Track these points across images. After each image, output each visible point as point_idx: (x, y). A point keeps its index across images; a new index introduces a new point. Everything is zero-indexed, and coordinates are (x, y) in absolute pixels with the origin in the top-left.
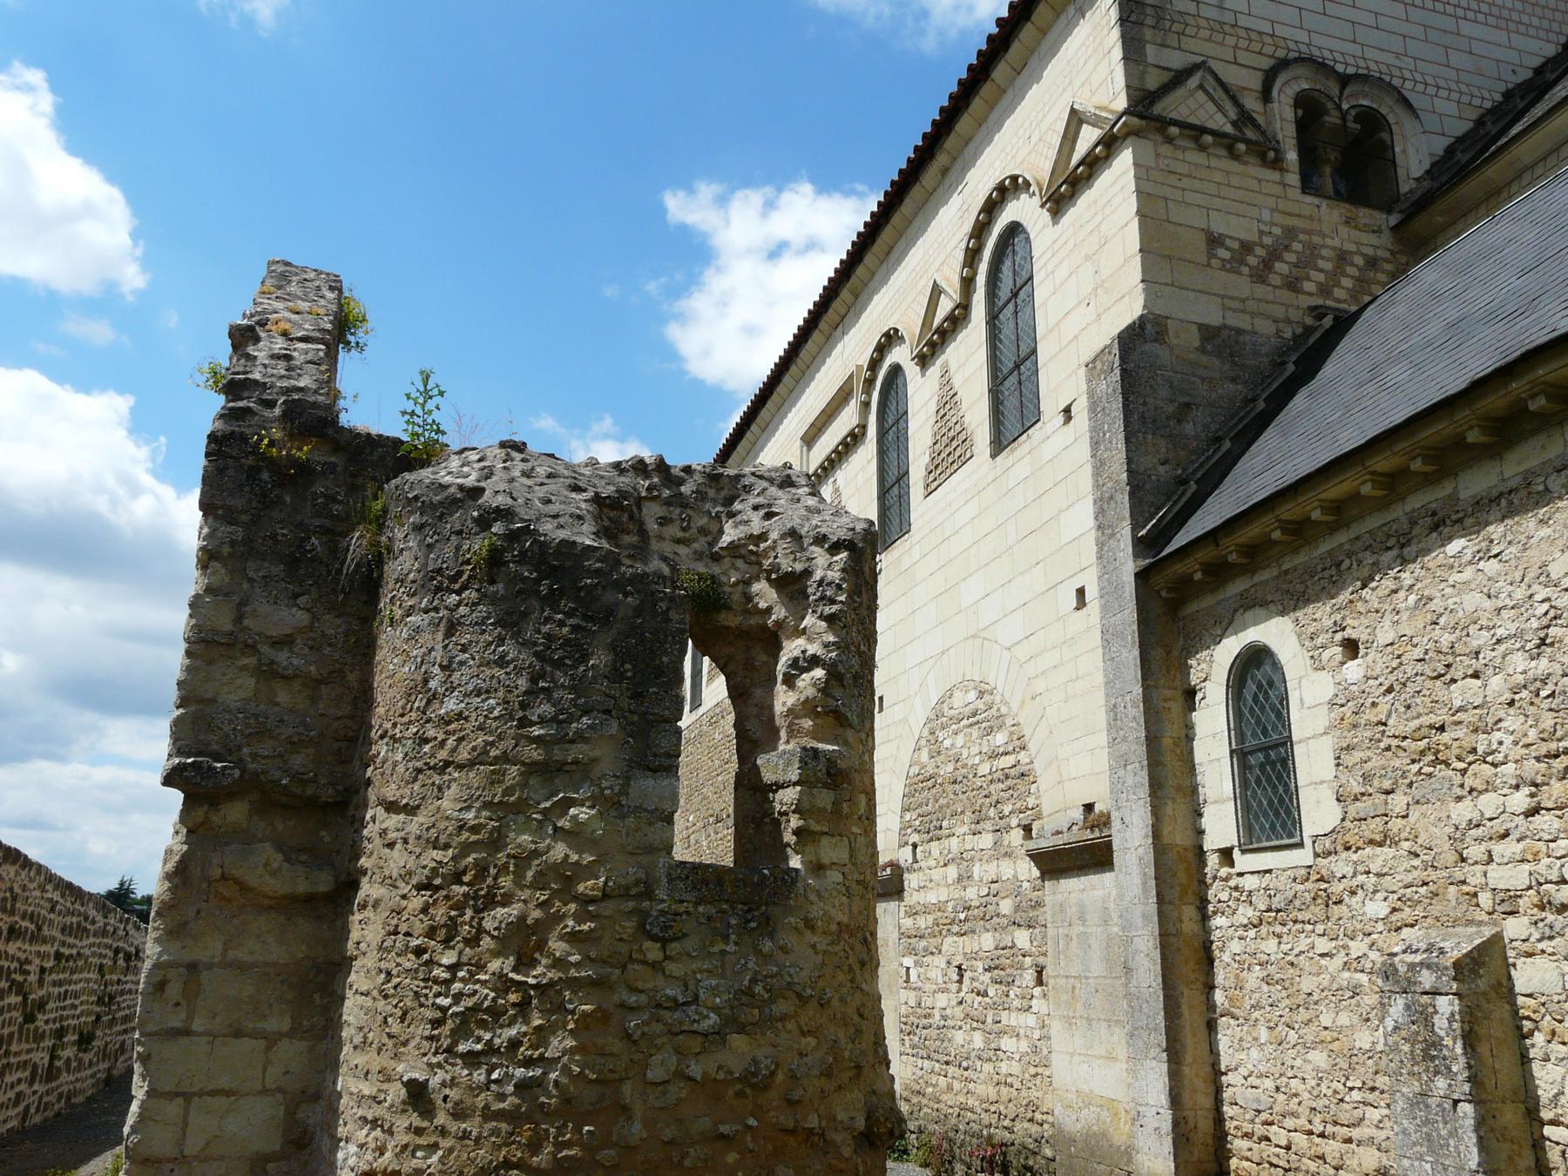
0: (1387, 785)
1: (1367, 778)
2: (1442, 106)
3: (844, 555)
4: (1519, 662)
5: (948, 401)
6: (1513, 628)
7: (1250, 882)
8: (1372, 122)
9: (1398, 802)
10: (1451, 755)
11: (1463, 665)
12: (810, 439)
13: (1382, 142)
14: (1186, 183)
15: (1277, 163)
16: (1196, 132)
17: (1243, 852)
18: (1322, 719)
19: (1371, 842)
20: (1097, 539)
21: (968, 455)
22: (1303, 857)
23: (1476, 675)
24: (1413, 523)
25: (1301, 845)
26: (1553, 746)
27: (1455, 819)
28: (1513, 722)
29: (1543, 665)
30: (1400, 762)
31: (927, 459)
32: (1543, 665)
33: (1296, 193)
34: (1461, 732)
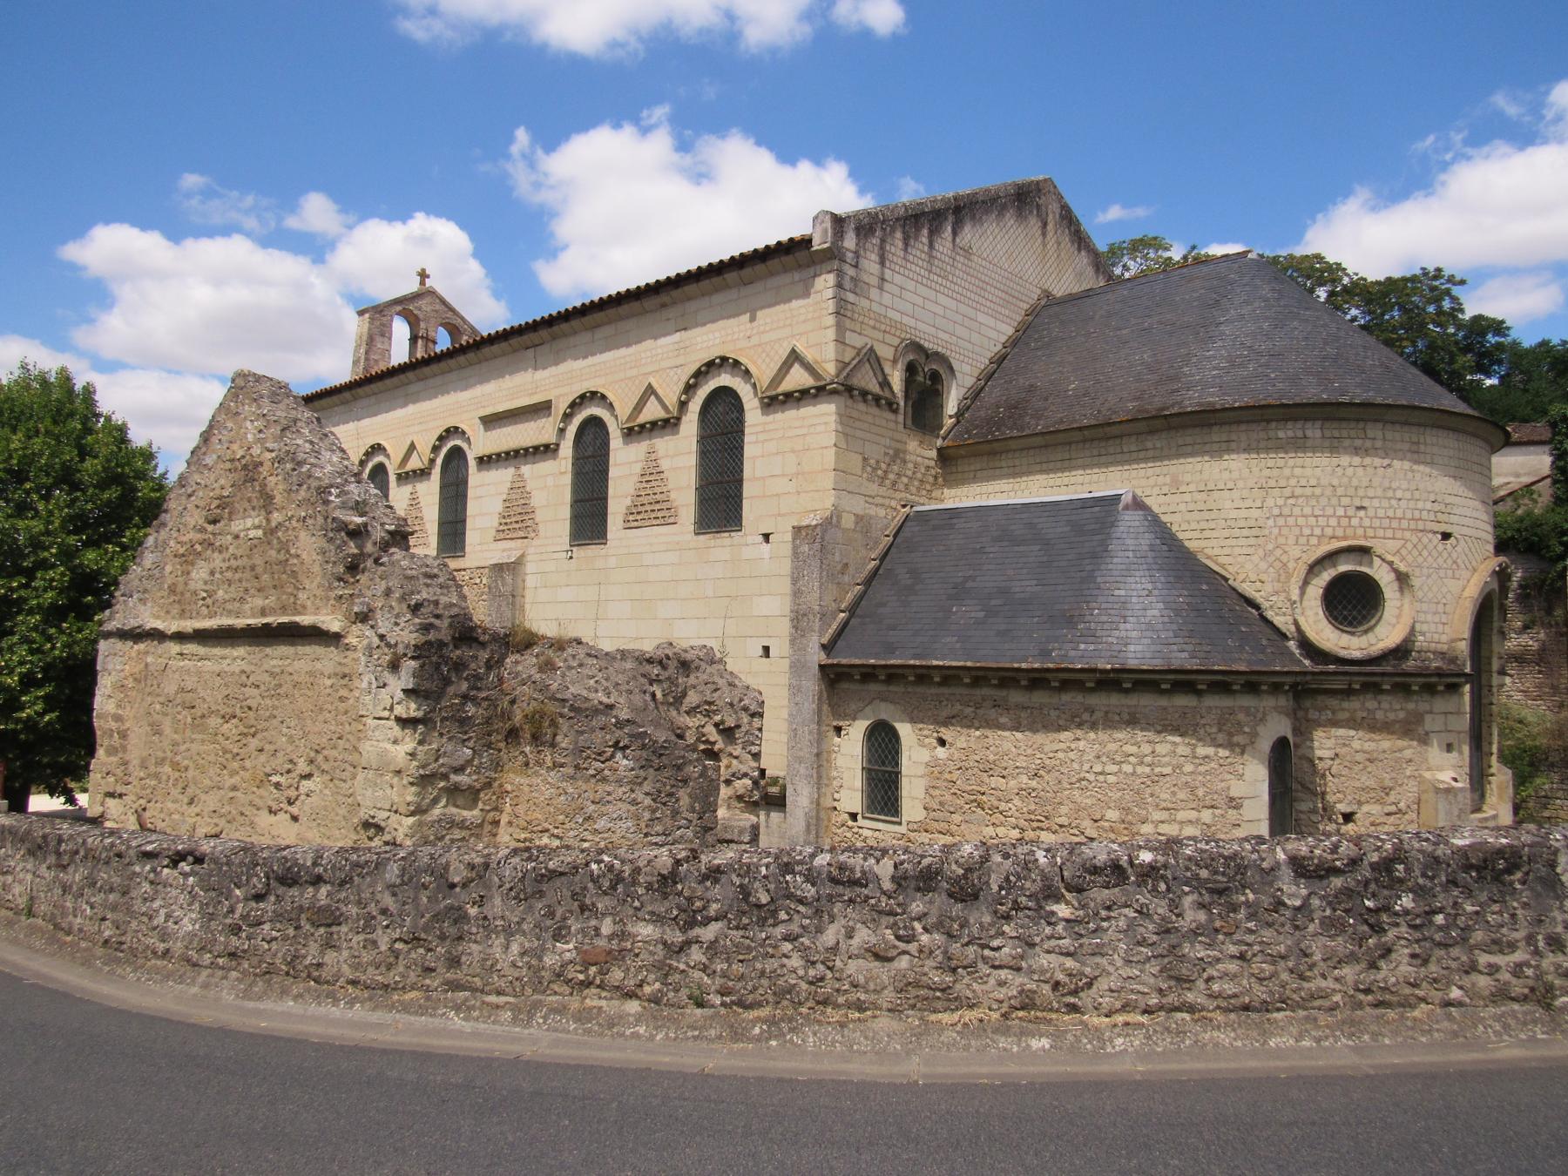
0: (952, 809)
1: (941, 804)
2: (966, 368)
3: (367, 315)
4: (1024, 779)
5: (652, 473)
6: (1024, 765)
7: (866, 833)
8: (935, 377)
9: (957, 818)
10: (986, 806)
11: (998, 771)
12: (492, 421)
13: (937, 390)
14: (858, 424)
15: (895, 411)
16: (864, 394)
17: (864, 818)
18: (921, 770)
19: (941, 832)
20: (791, 635)
21: (671, 520)
22: (903, 829)
23: (1003, 777)
24: (984, 700)
25: (900, 824)
26: (1033, 817)
27: (985, 833)
28: (1017, 801)
29: (1034, 784)
30: (961, 802)
31: (628, 502)
32: (1034, 784)
33: (901, 427)
34: (992, 798)
